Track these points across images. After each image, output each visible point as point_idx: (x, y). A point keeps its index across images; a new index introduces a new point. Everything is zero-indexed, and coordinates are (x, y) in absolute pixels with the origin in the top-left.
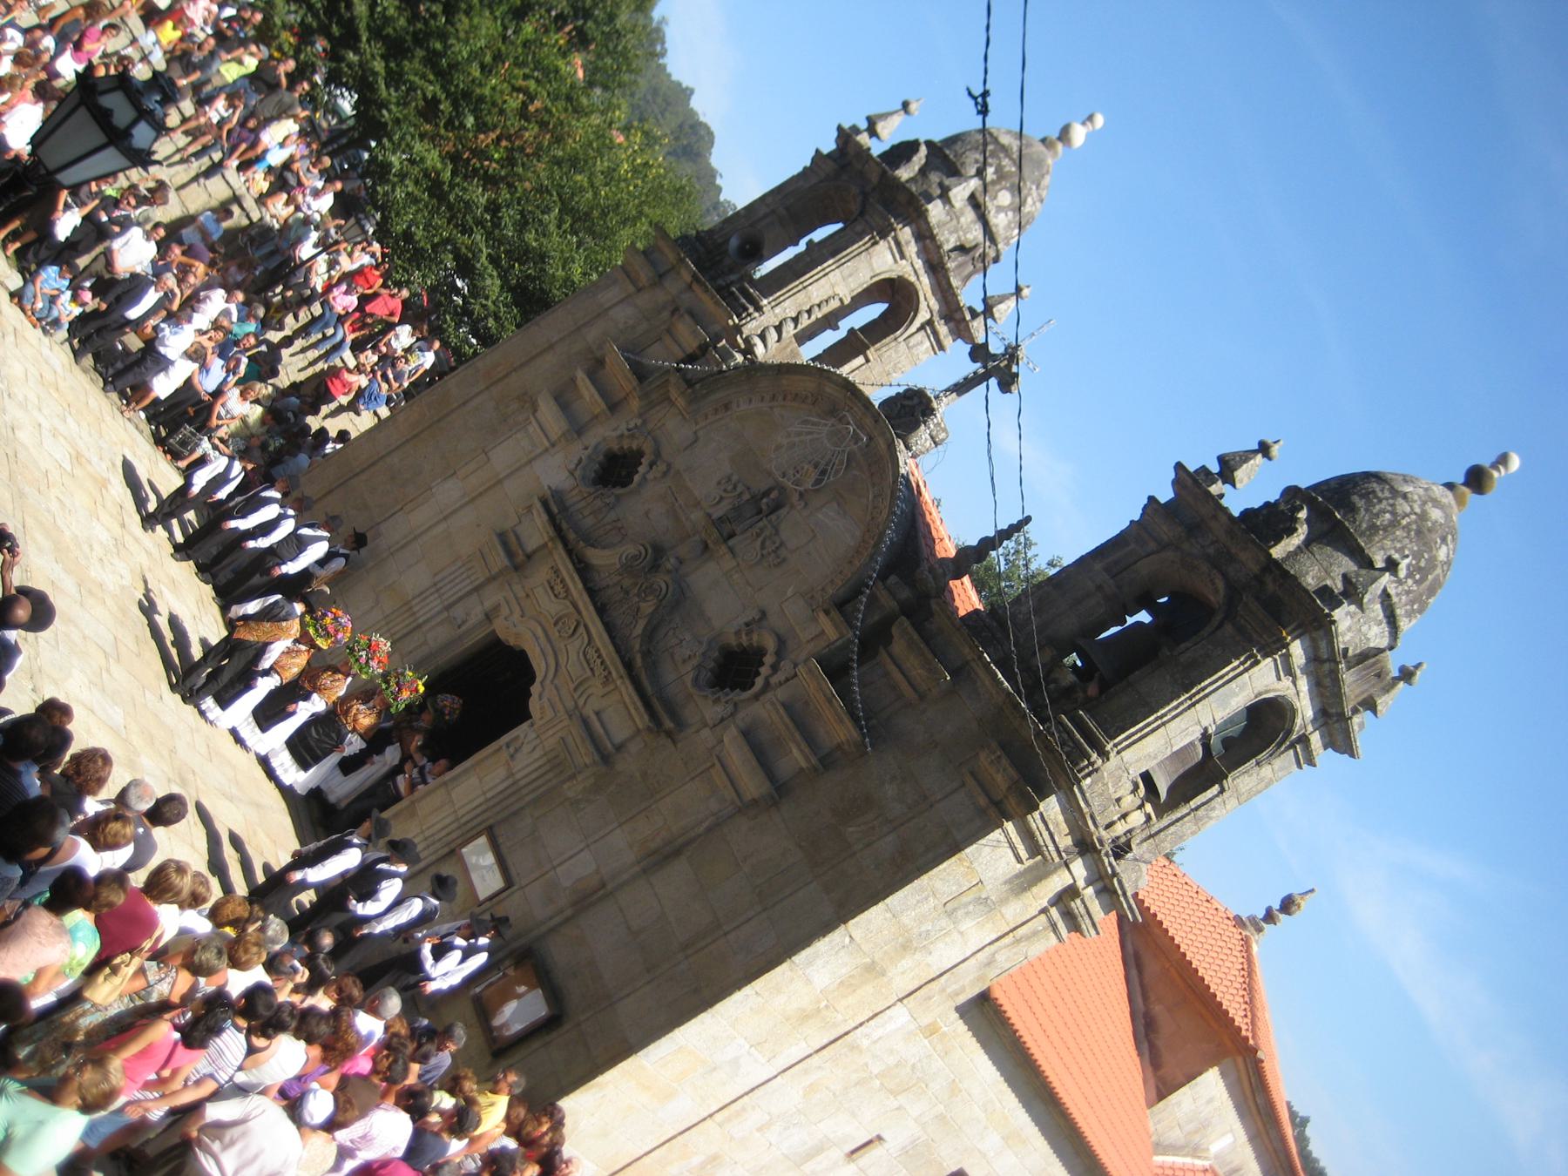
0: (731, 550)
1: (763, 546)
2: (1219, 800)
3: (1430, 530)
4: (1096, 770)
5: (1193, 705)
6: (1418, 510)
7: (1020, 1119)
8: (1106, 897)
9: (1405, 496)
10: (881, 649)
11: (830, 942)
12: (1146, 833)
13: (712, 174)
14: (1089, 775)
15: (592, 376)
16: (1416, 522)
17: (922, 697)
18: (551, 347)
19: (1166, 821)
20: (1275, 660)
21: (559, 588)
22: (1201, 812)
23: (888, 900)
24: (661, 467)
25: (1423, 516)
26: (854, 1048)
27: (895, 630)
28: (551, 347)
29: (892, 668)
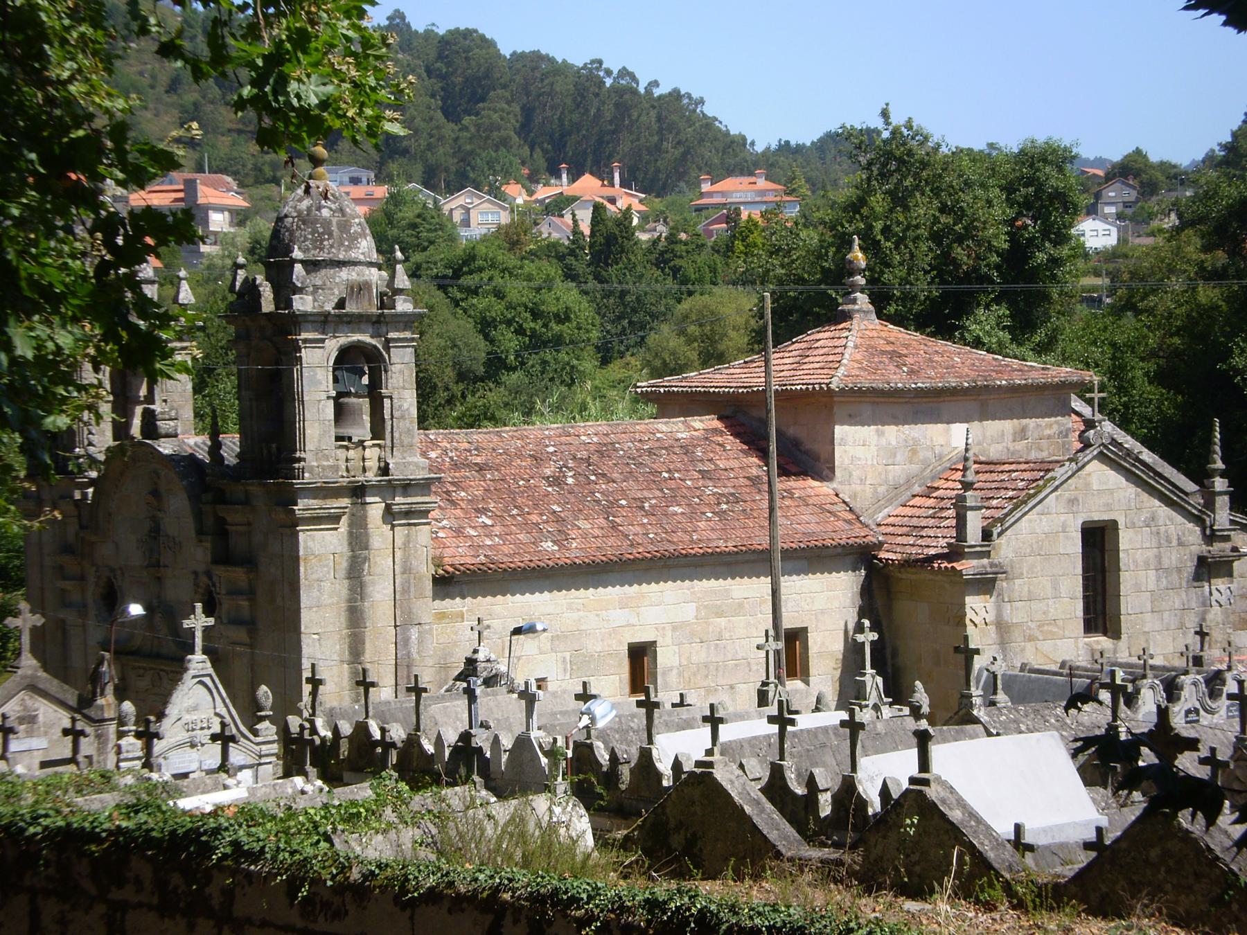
0: (165, 566)
1: (170, 549)
2: (395, 401)
3: (308, 215)
4: (303, 469)
5: (303, 401)
6: (295, 214)
7: (613, 593)
8: (410, 490)
9: (286, 216)
10: (228, 527)
11: (308, 645)
12: (388, 450)
13: (533, 62)
14: (303, 473)
15: (64, 578)
16: (299, 220)
17: (249, 524)
18: (42, 589)
19: (388, 436)
20: (305, 347)
21: (141, 672)
22: (396, 414)
23: (302, 605)
24: (119, 572)
25: (300, 213)
26: (519, 658)
27: (220, 515)
28: (42, 589)
29: (234, 528)
